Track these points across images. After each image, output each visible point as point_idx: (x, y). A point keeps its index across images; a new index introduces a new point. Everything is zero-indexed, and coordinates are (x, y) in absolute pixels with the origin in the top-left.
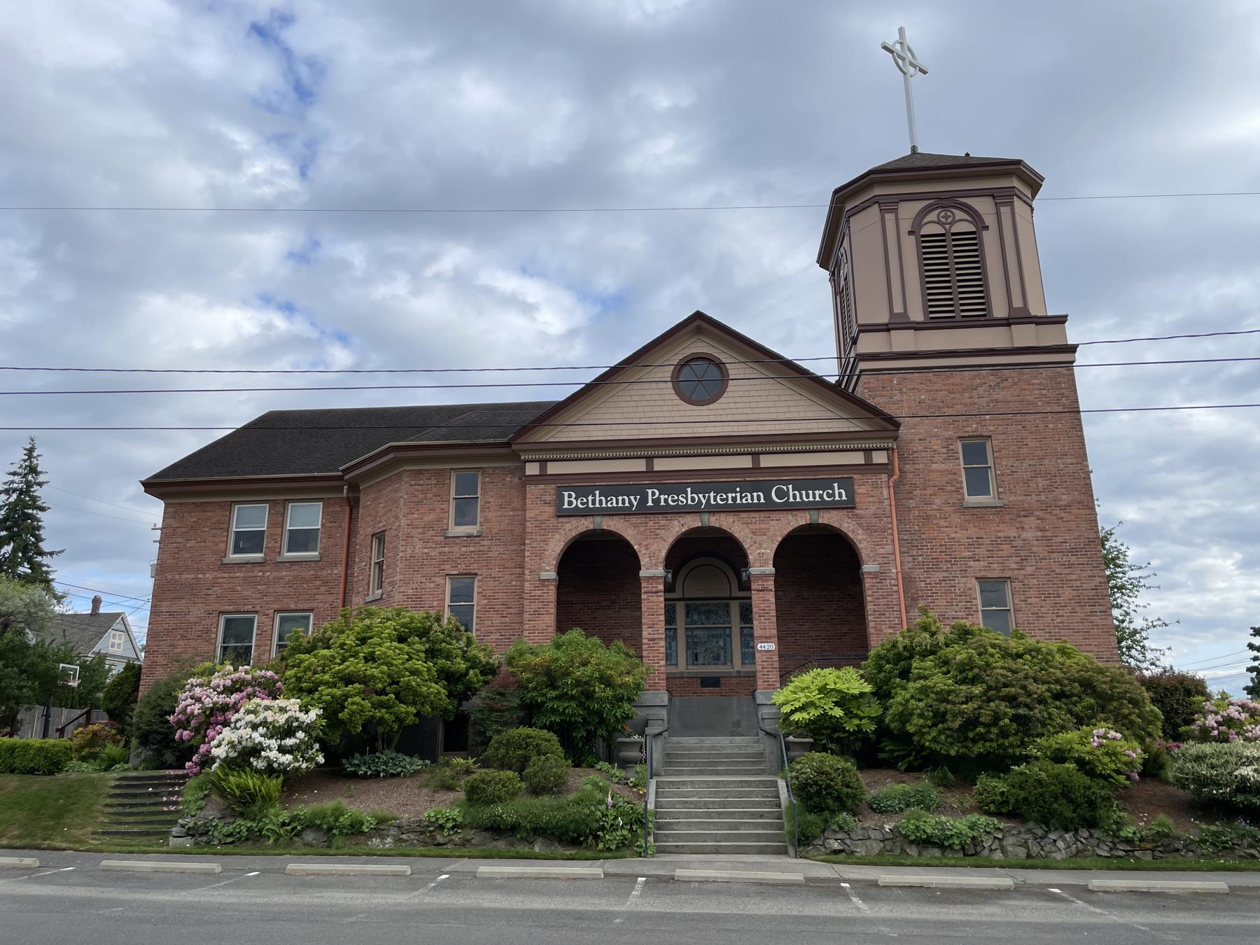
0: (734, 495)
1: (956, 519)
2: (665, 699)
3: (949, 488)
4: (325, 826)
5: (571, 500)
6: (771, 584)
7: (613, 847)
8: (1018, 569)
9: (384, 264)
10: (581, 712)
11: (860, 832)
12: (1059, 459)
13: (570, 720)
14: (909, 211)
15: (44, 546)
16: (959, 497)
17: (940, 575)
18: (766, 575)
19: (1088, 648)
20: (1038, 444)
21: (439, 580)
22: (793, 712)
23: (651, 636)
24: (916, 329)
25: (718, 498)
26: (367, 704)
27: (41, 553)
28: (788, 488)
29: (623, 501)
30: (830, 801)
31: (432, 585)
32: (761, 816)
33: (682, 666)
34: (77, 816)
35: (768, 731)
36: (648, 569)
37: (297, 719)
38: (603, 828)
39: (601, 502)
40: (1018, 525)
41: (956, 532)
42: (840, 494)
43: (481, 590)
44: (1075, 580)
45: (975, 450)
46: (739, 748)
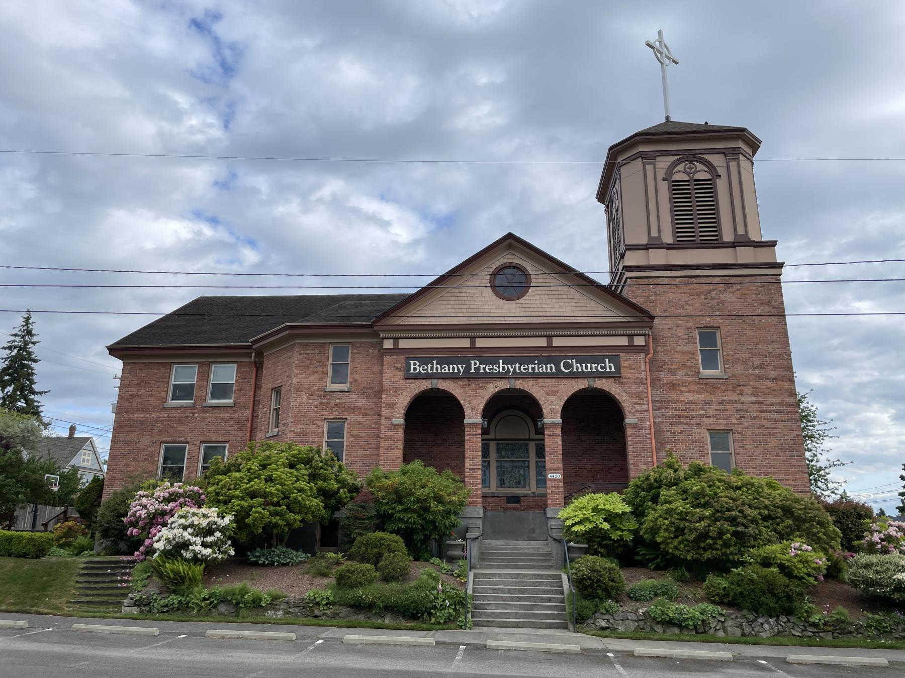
0: (533, 366)
1: (694, 386)
2: (481, 512)
3: (689, 364)
4: (234, 601)
5: (416, 367)
6: (559, 431)
7: (442, 621)
8: (738, 424)
9: (282, 191)
10: (420, 521)
11: (621, 614)
12: (769, 344)
13: (412, 527)
14: (663, 163)
15: (36, 387)
16: (696, 370)
17: (681, 427)
18: (555, 424)
19: (787, 482)
20: (754, 334)
21: (319, 423)
22: (573, 525)
23: (472, 467)
24: (667, 249)
25: (522, 368)
26: (266, 513)
27: (34, 393)
28: (572, 362)
29: (453, 368)
30: (600, 592)
31: (314, 426)
32: (549, 600)
33: (493, 488)
34: (56, 590)
35: (555, 537)
36: (470, 418)
37: (215, 523)
38: (435, 607)
39: (437, 369)
40: (738, 392)
41: (693, 396)
42: (610, 366)
43: (349, 431)
44: (779, 433)
45: (708, 337)
46: (534, 549)
